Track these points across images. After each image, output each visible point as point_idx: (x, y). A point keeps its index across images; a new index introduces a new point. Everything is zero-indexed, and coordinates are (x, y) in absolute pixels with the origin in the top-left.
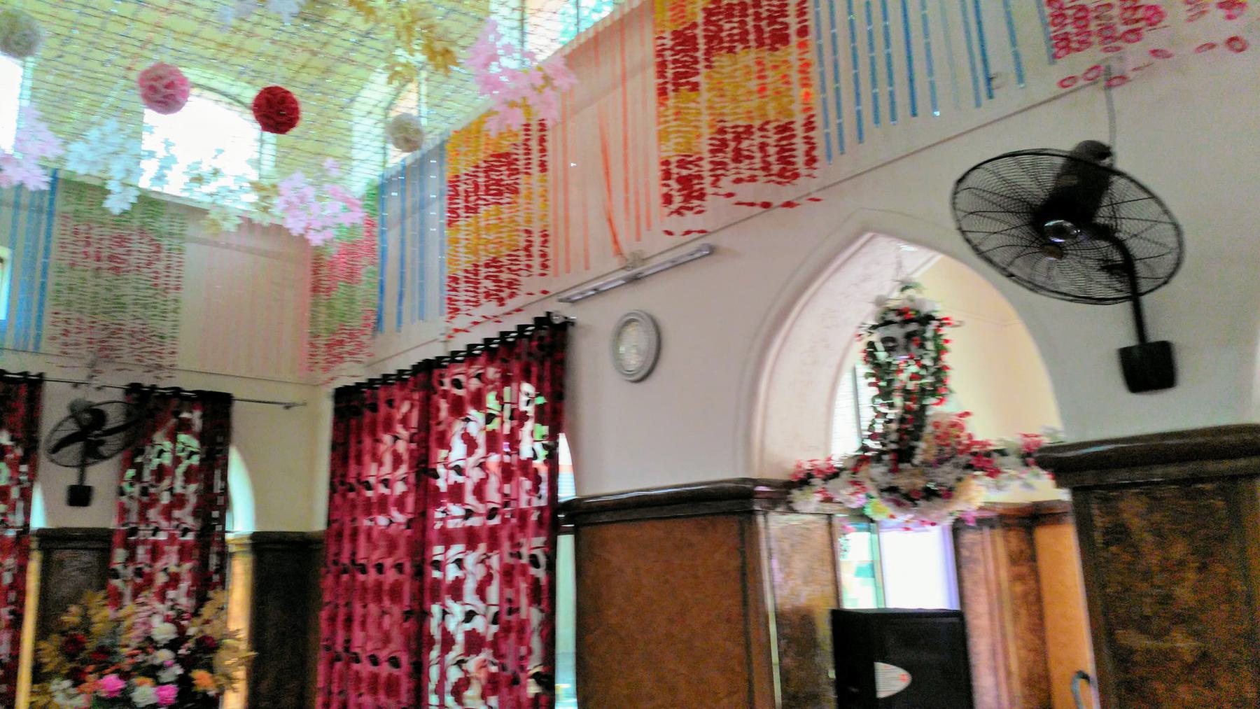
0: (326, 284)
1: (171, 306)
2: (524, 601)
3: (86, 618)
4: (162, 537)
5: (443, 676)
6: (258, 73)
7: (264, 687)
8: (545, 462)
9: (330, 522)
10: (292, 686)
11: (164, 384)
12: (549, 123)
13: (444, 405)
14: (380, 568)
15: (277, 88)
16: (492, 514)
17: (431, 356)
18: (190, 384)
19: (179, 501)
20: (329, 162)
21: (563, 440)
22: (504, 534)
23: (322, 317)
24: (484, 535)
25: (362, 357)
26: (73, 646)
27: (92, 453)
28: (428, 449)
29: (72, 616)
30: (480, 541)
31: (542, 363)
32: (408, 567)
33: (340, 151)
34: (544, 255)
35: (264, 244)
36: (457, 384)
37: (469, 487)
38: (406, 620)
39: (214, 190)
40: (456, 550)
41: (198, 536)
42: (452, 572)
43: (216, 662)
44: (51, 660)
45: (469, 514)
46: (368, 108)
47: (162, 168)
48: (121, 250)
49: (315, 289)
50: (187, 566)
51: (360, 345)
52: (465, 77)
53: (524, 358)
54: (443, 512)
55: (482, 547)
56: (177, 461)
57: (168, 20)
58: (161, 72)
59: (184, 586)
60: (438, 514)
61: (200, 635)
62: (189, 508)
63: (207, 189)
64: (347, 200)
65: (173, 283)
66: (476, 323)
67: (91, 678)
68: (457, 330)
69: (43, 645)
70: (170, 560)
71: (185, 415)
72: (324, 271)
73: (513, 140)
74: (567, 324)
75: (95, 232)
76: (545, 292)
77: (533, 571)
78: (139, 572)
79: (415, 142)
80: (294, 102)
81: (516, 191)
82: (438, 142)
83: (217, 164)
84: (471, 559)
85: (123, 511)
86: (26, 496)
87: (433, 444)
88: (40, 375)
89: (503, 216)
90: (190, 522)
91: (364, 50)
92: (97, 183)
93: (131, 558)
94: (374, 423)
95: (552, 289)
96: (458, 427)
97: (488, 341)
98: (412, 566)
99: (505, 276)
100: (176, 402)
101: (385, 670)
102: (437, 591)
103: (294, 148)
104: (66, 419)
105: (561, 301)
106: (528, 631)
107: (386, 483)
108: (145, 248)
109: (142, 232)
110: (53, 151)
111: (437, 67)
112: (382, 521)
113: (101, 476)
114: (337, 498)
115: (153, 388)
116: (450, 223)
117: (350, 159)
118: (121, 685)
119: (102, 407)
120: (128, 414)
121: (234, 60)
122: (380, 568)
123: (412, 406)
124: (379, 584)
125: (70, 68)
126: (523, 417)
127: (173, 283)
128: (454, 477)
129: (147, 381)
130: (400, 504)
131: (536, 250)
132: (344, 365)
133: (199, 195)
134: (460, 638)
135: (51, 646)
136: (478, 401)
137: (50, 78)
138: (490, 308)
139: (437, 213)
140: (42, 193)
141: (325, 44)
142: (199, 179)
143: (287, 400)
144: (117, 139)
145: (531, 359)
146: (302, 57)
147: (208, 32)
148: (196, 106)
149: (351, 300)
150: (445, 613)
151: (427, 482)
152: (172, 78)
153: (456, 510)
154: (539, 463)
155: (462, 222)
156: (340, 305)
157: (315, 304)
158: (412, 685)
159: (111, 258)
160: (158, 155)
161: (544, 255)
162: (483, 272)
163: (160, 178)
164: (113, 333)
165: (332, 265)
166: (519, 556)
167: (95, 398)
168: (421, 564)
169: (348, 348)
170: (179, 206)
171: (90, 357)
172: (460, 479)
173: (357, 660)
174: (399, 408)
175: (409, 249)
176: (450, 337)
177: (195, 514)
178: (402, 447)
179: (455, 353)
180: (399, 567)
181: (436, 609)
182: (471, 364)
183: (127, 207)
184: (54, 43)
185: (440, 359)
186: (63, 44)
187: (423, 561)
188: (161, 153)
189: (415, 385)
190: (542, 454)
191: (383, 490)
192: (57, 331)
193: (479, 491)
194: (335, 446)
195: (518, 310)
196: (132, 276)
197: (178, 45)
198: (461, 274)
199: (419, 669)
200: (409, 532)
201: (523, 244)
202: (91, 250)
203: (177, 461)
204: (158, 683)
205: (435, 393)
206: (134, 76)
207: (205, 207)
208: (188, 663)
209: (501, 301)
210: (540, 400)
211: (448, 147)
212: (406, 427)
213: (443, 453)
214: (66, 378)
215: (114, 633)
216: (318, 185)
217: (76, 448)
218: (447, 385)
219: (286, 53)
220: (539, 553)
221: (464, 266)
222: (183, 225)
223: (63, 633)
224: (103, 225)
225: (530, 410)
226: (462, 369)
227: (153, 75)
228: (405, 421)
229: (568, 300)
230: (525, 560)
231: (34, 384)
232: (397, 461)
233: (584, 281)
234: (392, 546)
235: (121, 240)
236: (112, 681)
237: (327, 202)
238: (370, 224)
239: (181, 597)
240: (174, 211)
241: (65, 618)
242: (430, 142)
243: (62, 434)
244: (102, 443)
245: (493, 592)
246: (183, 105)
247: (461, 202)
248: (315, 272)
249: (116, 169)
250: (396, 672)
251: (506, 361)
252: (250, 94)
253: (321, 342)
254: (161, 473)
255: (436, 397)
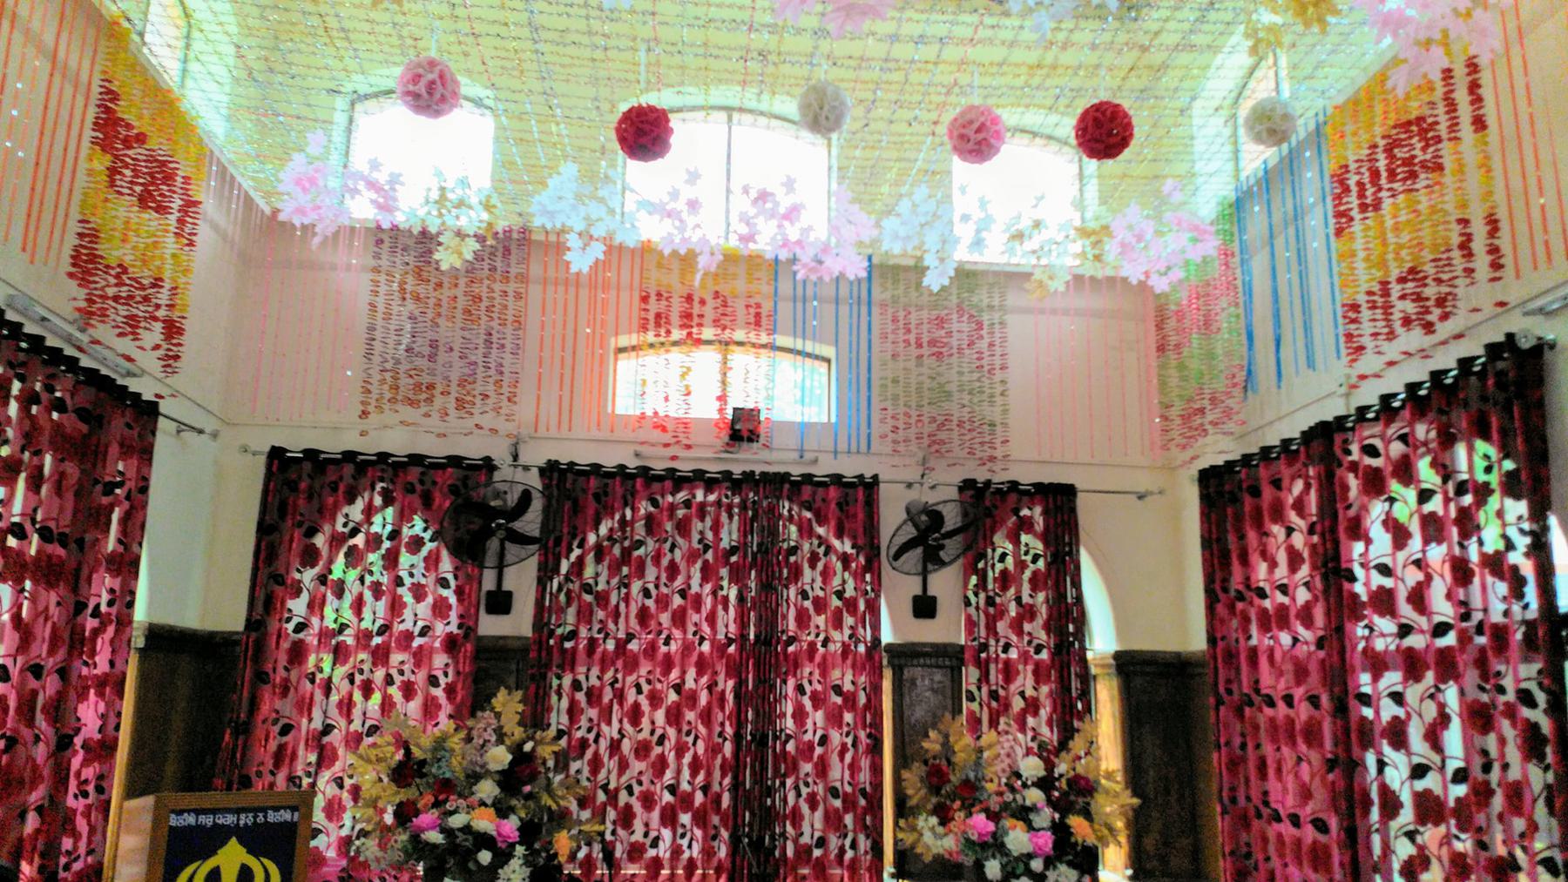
0: (1173, 339)
1: (999, 389)
2: (1513, 754)
3: (946, 744)
4: (1013, 654)
5: (1387, 850)
6: (1078, 91)
7: (1149, 843)
8: (1527, 555)
9: (1212, 640)
10: (1185, 842)
11: (1000, 477)
12: (1483, 61)
13: (1353, 482)
14: (1289, 700)
15: (1102, 104)
16: (1441, 629)
17: (1329, 417)
19: (1028, 613)
20: (1169, 183)
21: (1553, 521)
22: (1464, 660)
23: (1173, 382)
24: (1431, 659)
25: (1230, 426)
26: (936, 777)
27: (932, 559)
28: (1336, 543)
29: (932, 744)
30: (1428, 668)
31: (1507, 409)
32: (1325, 700)
33: (1181, 168)
34: (1494, 250)
35: (1096, 302)
36: (1371, 451)
37: (1402, 595)
38: (1330, 770)
39: (1036, 247)
40: (1392, 679)
41: (1053, 655)
42: (1389, 710)
43: (1093, 808)
44: (915, 791)
45: (1405, 630)
46: (1216, 103)
47: (978, 231)
48: (943, 333)
49: (1161, 349)
50: (1045, 689)
51: (1228, 413)
52: (1347, 30)
53: (1475, 405)
54: (1366, 626)
55: (1430, 677)
56: (1021, 566)
57: (974, 53)
58: (968, 117)
59: (1044, 713)
60: (1361, 631)
61: (1072, 773)
62: (1040, 621)
63: (1029, 245)
64: (1196, 228)
65: (998, 362)
66: (1391, 364)
67: (960, 815)
68: (1363, 377)
69: (906, 774)
70: (1025, 681)
71: (1025, 512)
72: (1172, 323)
73: (1426, 98)
74: (1541, 349)
75: (913, 319)
76: (1502, 304)
77: (1526, 712)
79: (1284, 132)
80: (1126, 115)
81: (1439, 168)
82: (1312, 126)
83: (1038, 214)
84: (1413, 693)
85: (971, 624)
86: (873, 608)
87: (1342, 536)
88: (875, 477)
89: (1420, 207)
90: (1042, 636)
91: (1206, 27)
92: (911, 263)
93: (984, 677)
94: (1258, 512)
95: (1512, 298)
96: (1378, 509)
97: (1412, 388)
98: (1332, 698)
99: (1431, 291)
100: (1013, 497)
101: (1309, 834)
102: (1366, 735)
103: (1125, 175)
104: (905, 522)
105: (1526, 314)
106: (1527, 798)
107: (1284, 589)
108: (965, 327)
109: (960, 310)
110: (867, 234)
111: (1307, 24)
112: (1285, 639)
113: (945, 583)
114: (1221, 609)
115: (988, 483)
116: (1339, 232)
117: (1193, 175)
118: (991, 827)
119: (939, 508)
120: (965, 514)
121: (1048, 83)
122: (1289, 700)
123: (1307, 486)
124: (1290, 722)
125: (876, 137)
126: (1483, 492)
127: (998, 362)
128: (1377, 580)
129: (981, 476)
130: (1306, 616)
131: (1479, 245)
132: (1209, 439)
133: (1020, 258)
134: (1406, 797)
135: (913, 777)
136: (1405, 471)
137: (858, 153)
138: (1414, 338)
139: (1318, 221)
140: (859, 281)
141: (1157, 34)
142: (1019, 236)
143: (1142, 489)
144: (931, 206)
145: (1489, 407)
146: (1130, 57)
147: (1018, 55)
148: (1011, 151)
149: (1210, 356)
150: (1381, 765)
151: (1340, 590)
152: (982, 119)
153: (1386, 625)
154: (1516, 558)
155: (1357, 227)
156: (1194, 365)
157: (1162, 367)
158: (1347, 859)
159: (932, 343)
160: (975, 218)
161: (1494, 250)
162: (1396, 290)
163: (978, 243)
164: (943, 424)
165: (1180, 315)
166: (1501, 690)
167: (931, 498)
168: (1344, 700)
169: (1210, 417)
170: (996, 274)
171: (920, 455)
172: (1388, 583)
173: (1279, 819)
174: (1290, 490)
175: (1283, 277)
176: (1354, 387)
177: (1047, 627)
178: (1298, 540)
179: (1362, 410)
180: (1314, 701)
181: (1371, 759)
182: (1387, 424)
183: (946, 282)
184: (859, 111)
185: (1340, 420)
186: (869, 111)
187: (1346, 692)
188: (977, 214)
189: (1308, 456)
190: (1522, 542)
191: (1281, 598)
192: (887, 428)
193: (1418, 598)
194: (1206, 543)
195: (1459, 336)
196: (954, 360)
197: (987, 81)
198: (1362, 299)
199: (1353, 837)
200: (1322, 654)
201: (1456, 240)
202: (912, 337)
203: (1021, 566)
204: (1030, 827)
205: (1340, 465)
206: (942, 130)
207: (1028, 269)
208: (1062, 806)
209: (1429, 328)
210: (1509, 465)
211: (1328, 130)
212: (1301, 513)
213: (1359, 547)
214: (899, 478)
215: (978, 764)
216: (1158, 217)
217: (915, 556)
218: (1356, 454)
219: (1109, 58)
220: (1532, 686)
221: (1365, 287)
222: (1003, 295)
223: (926, 762)
224: (920, 308)
225: (1494, 479)
226: (1377, 429)
227: (960, 121)
228: (1299, 506)
229: (1541, 311)
230: (1510, 696)
231: (870, 486)
232: (1295, 560)
233: (1535, 292)
234: (1301, 673)
235: (941, 322)
236: (980, 822)
237: (1168, 237)
238: (1227, 254)
239: (1042, 725)
240: (991, 280)
241: (926, 745)
242: (1303, 127)
243: (901, 539)
244: (942, 547)
245: (1453, 738)
246: (998, 150)
247: (1353, 200)
248: (1159, 327)
249: (932, 240)
250: (1322, 838)
251: (1447, 413)
252: (1067, 126)
253: (1174, 412)
254: (1005, 580)
255: (1339, 472)
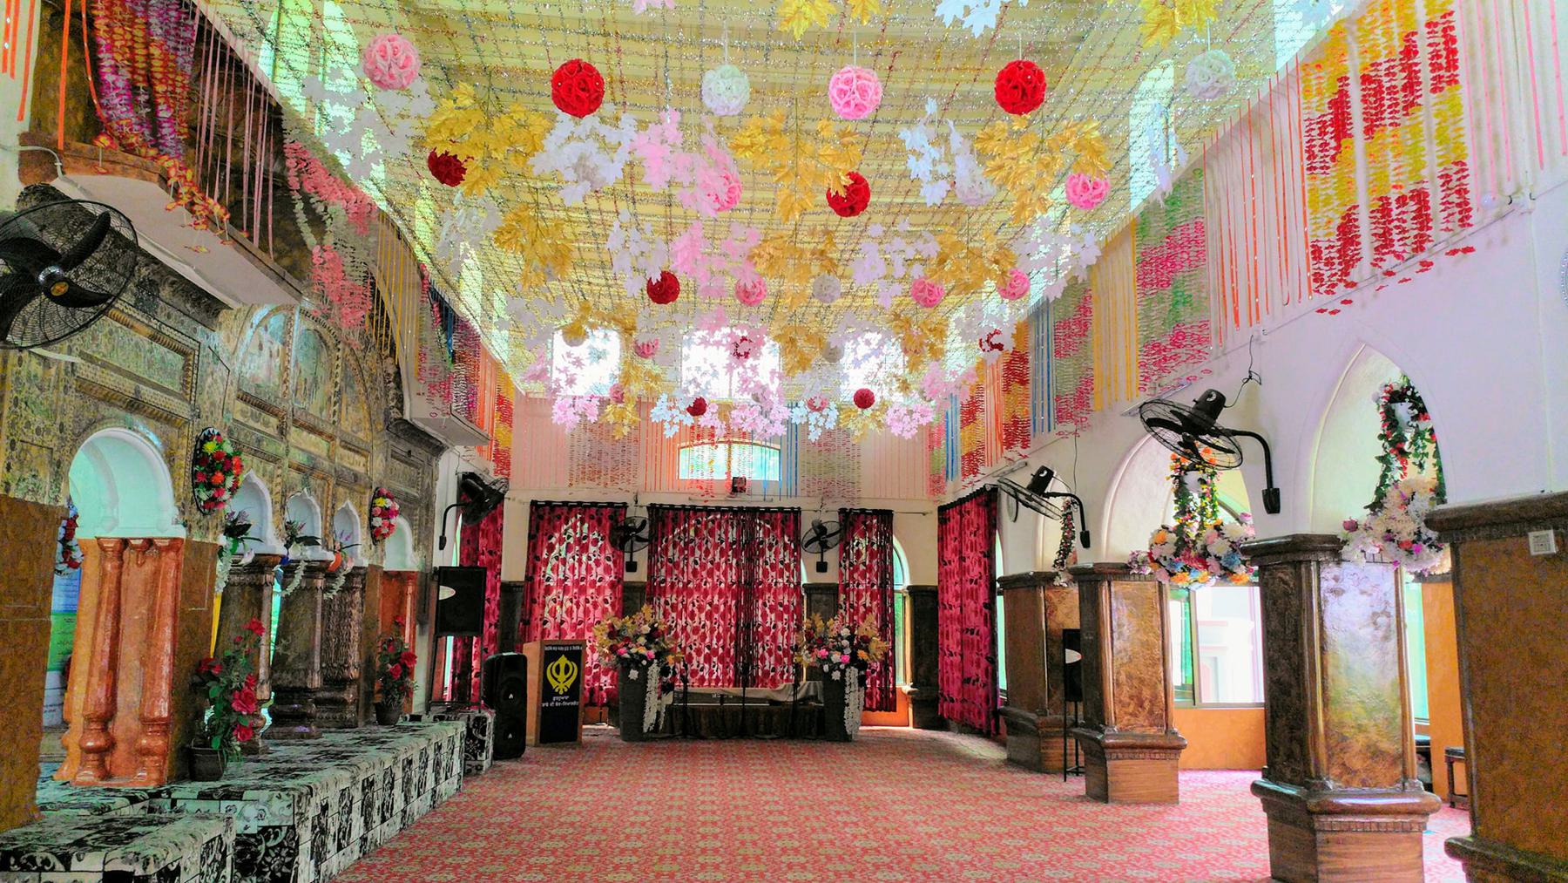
7: (921, 671)
11: (857, 507)
18: (870, 506)
27: (824, 547)
78: (852, 606)
85: (841, 575)
86: (798, 568)
93: (848, 598)
113: (832, 556)
129: (848, 507)
159: (825, 444)
231: (796, 513)
236: (823, 652)
